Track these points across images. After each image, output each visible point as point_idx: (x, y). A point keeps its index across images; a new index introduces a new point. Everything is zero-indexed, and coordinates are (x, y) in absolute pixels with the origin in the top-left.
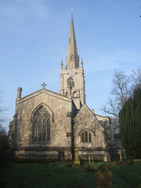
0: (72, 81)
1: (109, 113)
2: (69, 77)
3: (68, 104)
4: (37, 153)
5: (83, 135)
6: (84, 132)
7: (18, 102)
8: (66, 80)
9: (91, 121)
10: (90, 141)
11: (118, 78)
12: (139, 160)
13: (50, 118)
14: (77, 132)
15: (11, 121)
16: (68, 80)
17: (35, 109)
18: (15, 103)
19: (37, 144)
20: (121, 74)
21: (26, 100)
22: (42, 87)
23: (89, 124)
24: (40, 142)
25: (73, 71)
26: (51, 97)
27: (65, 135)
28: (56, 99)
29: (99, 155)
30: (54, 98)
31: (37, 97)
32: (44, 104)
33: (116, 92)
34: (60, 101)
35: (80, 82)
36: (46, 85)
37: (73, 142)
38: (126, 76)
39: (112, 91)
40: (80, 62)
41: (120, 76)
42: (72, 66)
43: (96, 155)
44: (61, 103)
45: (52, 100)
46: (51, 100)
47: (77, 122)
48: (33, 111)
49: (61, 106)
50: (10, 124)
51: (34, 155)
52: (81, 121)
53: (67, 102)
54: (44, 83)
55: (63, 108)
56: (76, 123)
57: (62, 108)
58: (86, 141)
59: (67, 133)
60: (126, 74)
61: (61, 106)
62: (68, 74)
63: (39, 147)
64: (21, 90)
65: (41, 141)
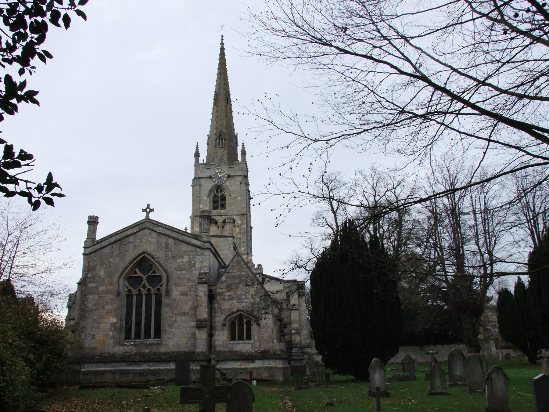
0: (219, 195)
1: (305, 269)
2: (214, 184)
3: (202, 254)
4: (131, 368)
5: (233, 324)
6: (235, 317)
7: (88, 251)
8: (206, 192)
9: (250, 293)
10: (249, 337)
11: (328, 187)
12: (1, 385)
13: (161, 286)
14: (220, 318)
15: (73, 292)
16: (210, 191)
17: (128, 266)
18: (82, 251)
19: (130, 347)
20: (334, 177)
21: (106, 244)
22: (143, 216)
23: (246, 298)
24: (138, 341)
25: (221, 170)
26: (163, 240)
27: (194, 324)
28: (176, 244)
29: (267, 368)
30: (171, 241)
31: (131, 239)
32: (147, 254)
33: (324, 220)
34: (184, 247)
35: (239, 198)
36: (152, 210)
37: (211, 340)
38: (345, 184)
39: (314, 217)
40: (239, 149)
41: (333, 183)
42: (221, 159)
43: (260, 368)
44: (185, 251)
45: (167, 245)
46: (163, 245)
47: (221, 294)
48: (121, 269)
49: (186, 259)
50: (70, 300)
51: (123, 372)
52: (229, 293)
53: (198, 249)
54: (148, 205)
55: (189, 263)
56: (218, 298)
57: (188, 262)
58: (241, 338)
59: (198, 321)
60: (345, 180)
61: (186, 259)
62: (210, 177)
63: (136, 354)
64: (93, 222)
65: (140, 338)
